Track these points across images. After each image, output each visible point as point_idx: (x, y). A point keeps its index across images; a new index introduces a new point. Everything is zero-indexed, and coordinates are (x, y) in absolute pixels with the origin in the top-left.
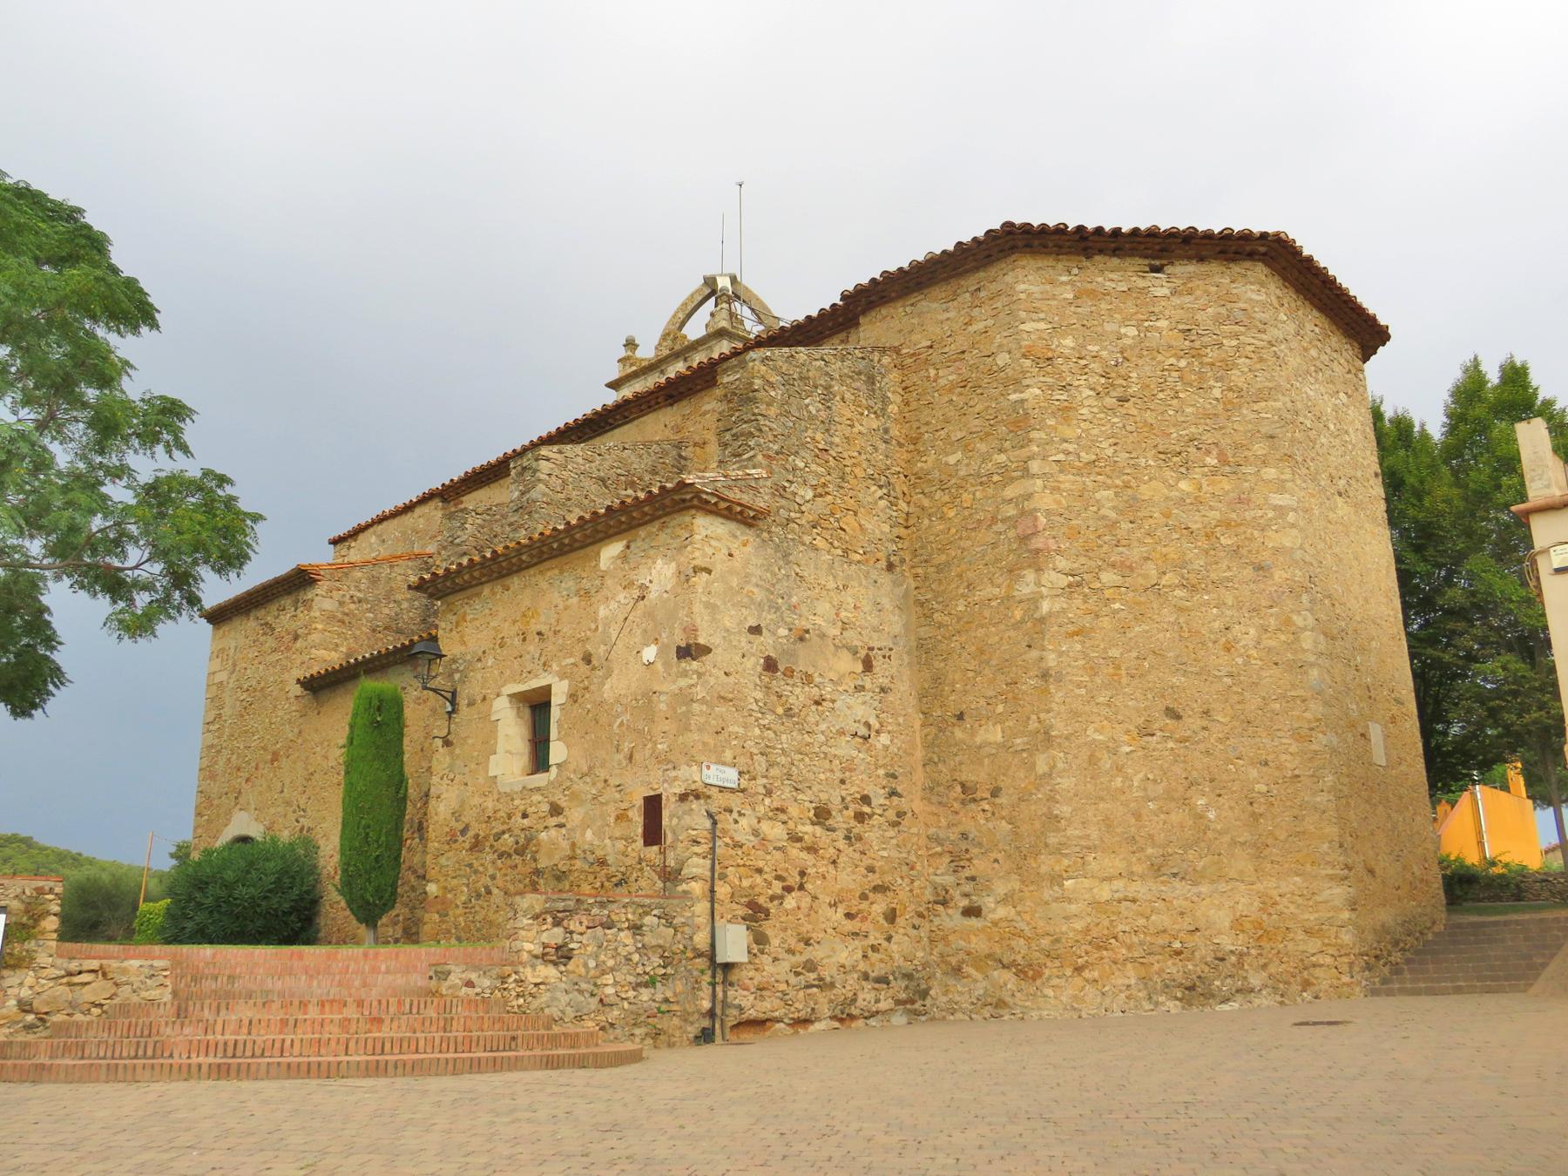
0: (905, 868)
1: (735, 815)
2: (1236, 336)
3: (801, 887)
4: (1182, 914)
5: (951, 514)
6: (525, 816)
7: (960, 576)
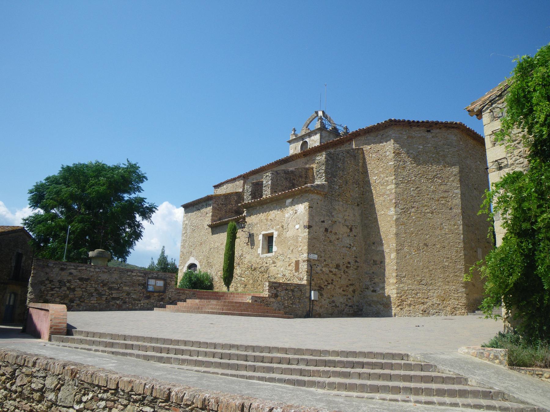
3: (332, 283)
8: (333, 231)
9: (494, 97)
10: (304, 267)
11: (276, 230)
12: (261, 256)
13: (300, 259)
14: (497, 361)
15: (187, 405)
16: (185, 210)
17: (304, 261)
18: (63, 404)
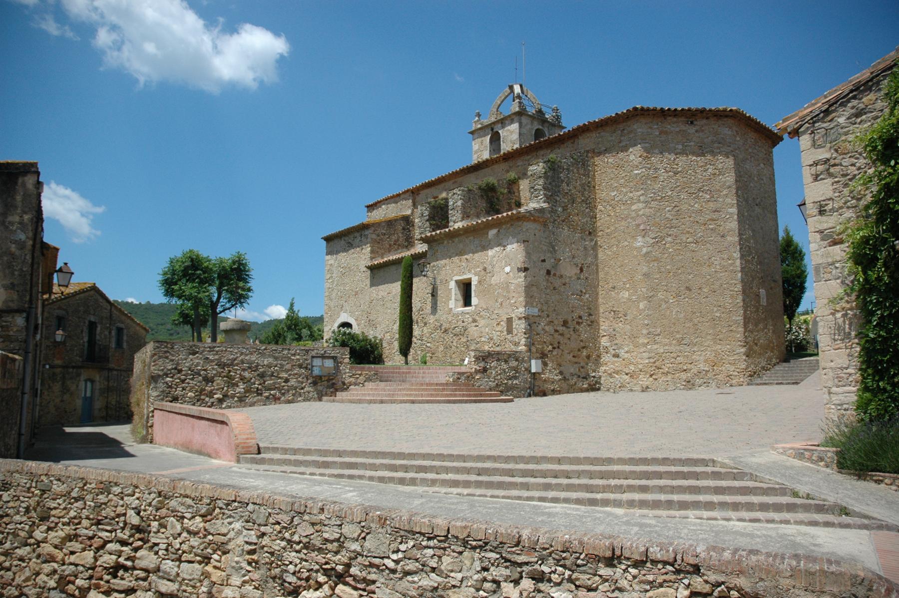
8: (558, 274)
9: (817, 113)
10: (520, 326)
11: (475, 274)
14: (822, 464)
15: (545, 549)
17: (520, 319)
18: (374, 554)
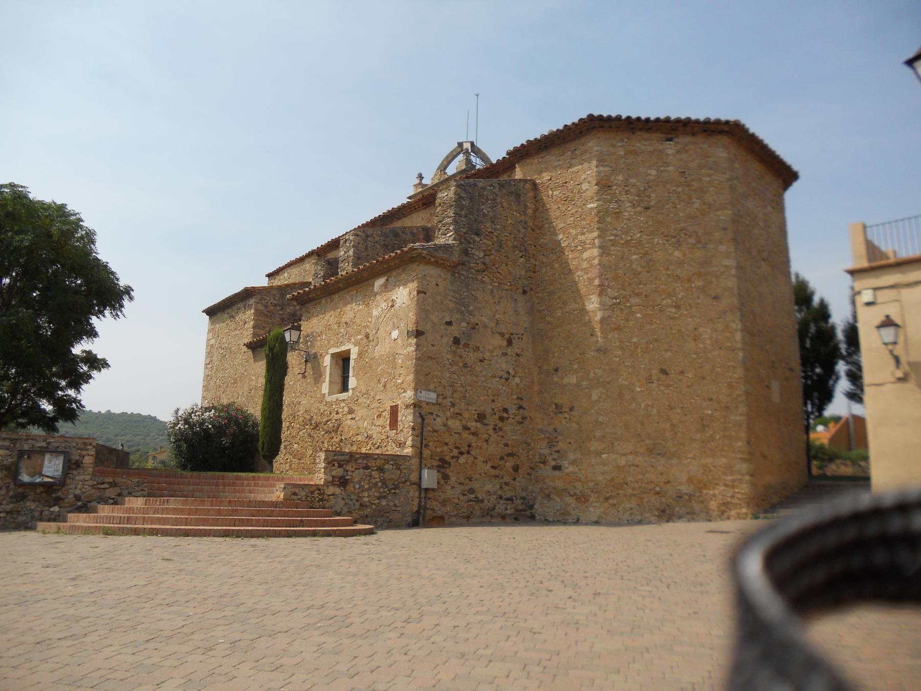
0: (525, 445)
1: (434, 416)
2: (709, 175)
3: (468, 453)
4: (662, 474)
5: (557, 266)
6: (337, 413)
7: (559, 298)
10: (407, 418)
12: (328, 399)
13: (399, 402)
16: (210, 319)
17: (407, 407)
